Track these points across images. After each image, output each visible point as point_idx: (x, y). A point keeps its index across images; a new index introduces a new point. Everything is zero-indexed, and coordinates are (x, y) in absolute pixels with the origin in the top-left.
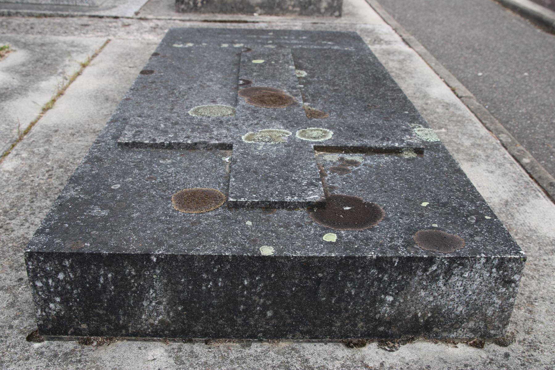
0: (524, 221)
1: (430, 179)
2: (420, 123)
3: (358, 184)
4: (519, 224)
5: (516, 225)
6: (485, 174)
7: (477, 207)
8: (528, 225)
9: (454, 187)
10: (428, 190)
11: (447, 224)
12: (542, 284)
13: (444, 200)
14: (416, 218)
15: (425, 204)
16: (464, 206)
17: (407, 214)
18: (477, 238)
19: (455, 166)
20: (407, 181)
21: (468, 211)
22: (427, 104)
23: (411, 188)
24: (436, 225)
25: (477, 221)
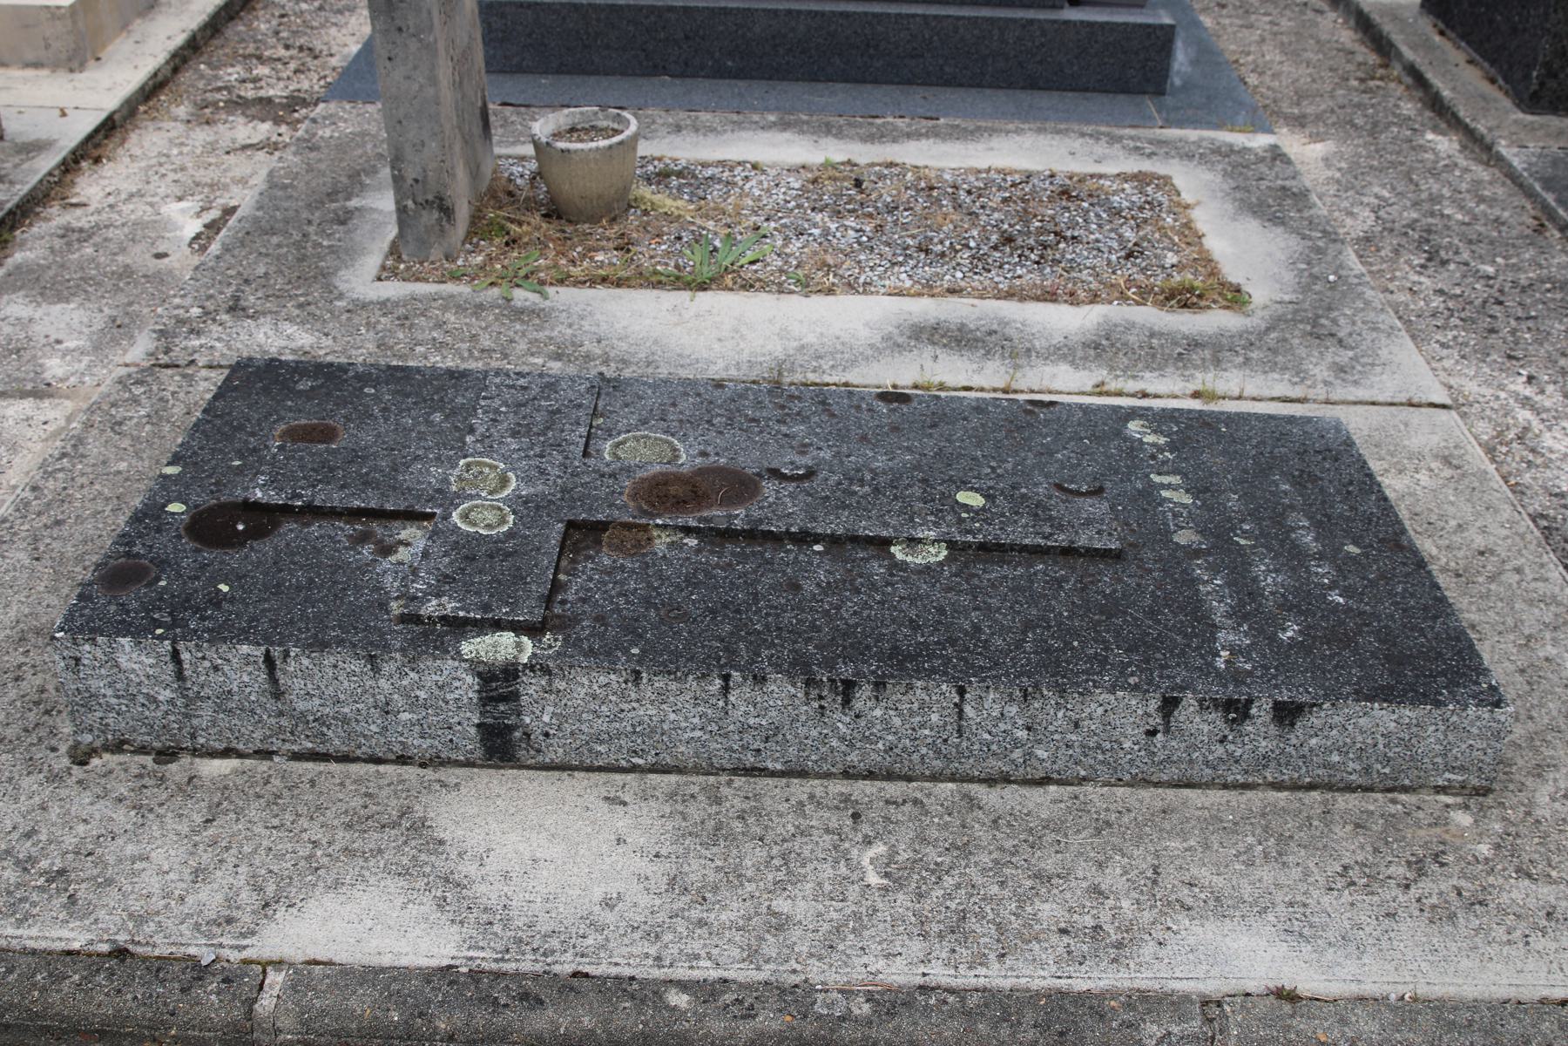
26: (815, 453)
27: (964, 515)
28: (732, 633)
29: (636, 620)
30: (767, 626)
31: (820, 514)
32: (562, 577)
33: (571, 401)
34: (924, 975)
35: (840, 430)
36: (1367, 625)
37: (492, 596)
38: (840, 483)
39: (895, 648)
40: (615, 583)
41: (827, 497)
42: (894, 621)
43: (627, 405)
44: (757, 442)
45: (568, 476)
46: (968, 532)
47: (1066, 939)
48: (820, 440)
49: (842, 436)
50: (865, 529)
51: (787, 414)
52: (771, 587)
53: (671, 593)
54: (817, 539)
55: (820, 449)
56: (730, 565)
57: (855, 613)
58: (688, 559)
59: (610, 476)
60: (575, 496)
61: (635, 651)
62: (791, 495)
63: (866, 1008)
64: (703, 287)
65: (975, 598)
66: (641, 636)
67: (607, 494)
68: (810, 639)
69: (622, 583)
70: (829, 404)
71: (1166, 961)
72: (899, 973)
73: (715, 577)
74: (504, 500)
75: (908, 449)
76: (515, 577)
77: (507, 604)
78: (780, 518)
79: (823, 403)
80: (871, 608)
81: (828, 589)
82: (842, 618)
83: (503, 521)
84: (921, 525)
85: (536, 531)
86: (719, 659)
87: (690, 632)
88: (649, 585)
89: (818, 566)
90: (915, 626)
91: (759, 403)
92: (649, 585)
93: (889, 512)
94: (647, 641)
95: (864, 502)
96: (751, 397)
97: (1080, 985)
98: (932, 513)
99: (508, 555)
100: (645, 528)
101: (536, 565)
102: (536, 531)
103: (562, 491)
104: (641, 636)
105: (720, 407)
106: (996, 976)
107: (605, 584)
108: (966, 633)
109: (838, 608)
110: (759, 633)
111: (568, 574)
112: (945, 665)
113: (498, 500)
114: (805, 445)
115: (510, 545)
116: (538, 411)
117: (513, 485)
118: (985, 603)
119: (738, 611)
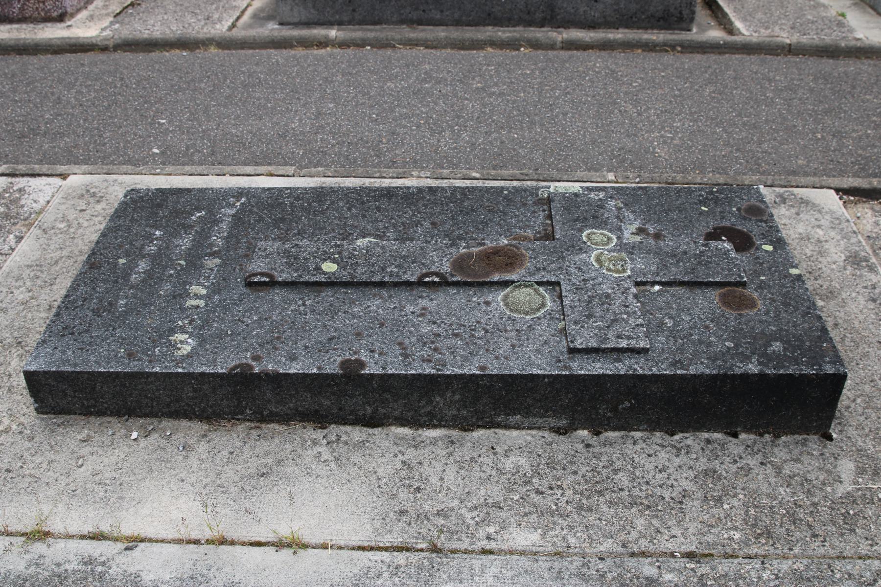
26: (416, 310)
27: (337, 256)
28: (463, 201)
29: (508, 205)
30: (447, 205)
31: (418, 251)
32: (549, 222)
33: (583, 327)
35: (398, 330)
37: (576, 201)
38: (404, 272)
39: (390, 199)
40: (522, 221)
41: (413, 263)
42: (388, 210)
43: (546, 342)
44: (454, 315)
45: (564, 268)
46: (338, 246)
48: (412, 320)
49: (397, 325)
50: (395, 244)
51: (433, 342)
52: (445, 223)
53: (494, 218)
55: (413, 313)
56: (467, 233)
57: (405, 213)
58: (488, 235)
59: (540, 269)
60: (555, 255)
61: (506, 192)
62: (433, 262)
63: (413, 173)
65: (345, 223)
66: (505, 198)
67: (538, 257)
68: (428, 201)
69: (518, 221)
70: (401, 355)
73: (474, 227)
74: (593, 250)
75: (354, 316)
76: (569, 209)
77: (567, 197)
78: (441, 248)
79: (406, 356)
80: (397, 216)
81: (417, 224)
82: (412, 210)
83: (588, 236)
84: (363, 249)
85: (569, 233)
86: (469, 191)
87: (483, 201)
88: (505, 221)
89: (421, 235)
90: (378, 209)
91: (452, 353)
92: (505, 221)
93: (379, 255)
94: (501, 197)
95: (392, 260)
96: (458, 358)
98: (355, 256)
99: (577, 220)
101: (562, 216)
102: (569, 233)
103: (563, 258)
104: (505, 198)
105: (480, 347)
107: (527, 220)
108: (355, 207)
109: (414, 215)
110: (451, 202)
111: (547, 224)
112: (369, 193)
113: (597, 249)
114: (422, 315)
115: (579, 225)
116: (601, 317)
117: (593, 260)
118: (341, 221)
119: (461, 211)
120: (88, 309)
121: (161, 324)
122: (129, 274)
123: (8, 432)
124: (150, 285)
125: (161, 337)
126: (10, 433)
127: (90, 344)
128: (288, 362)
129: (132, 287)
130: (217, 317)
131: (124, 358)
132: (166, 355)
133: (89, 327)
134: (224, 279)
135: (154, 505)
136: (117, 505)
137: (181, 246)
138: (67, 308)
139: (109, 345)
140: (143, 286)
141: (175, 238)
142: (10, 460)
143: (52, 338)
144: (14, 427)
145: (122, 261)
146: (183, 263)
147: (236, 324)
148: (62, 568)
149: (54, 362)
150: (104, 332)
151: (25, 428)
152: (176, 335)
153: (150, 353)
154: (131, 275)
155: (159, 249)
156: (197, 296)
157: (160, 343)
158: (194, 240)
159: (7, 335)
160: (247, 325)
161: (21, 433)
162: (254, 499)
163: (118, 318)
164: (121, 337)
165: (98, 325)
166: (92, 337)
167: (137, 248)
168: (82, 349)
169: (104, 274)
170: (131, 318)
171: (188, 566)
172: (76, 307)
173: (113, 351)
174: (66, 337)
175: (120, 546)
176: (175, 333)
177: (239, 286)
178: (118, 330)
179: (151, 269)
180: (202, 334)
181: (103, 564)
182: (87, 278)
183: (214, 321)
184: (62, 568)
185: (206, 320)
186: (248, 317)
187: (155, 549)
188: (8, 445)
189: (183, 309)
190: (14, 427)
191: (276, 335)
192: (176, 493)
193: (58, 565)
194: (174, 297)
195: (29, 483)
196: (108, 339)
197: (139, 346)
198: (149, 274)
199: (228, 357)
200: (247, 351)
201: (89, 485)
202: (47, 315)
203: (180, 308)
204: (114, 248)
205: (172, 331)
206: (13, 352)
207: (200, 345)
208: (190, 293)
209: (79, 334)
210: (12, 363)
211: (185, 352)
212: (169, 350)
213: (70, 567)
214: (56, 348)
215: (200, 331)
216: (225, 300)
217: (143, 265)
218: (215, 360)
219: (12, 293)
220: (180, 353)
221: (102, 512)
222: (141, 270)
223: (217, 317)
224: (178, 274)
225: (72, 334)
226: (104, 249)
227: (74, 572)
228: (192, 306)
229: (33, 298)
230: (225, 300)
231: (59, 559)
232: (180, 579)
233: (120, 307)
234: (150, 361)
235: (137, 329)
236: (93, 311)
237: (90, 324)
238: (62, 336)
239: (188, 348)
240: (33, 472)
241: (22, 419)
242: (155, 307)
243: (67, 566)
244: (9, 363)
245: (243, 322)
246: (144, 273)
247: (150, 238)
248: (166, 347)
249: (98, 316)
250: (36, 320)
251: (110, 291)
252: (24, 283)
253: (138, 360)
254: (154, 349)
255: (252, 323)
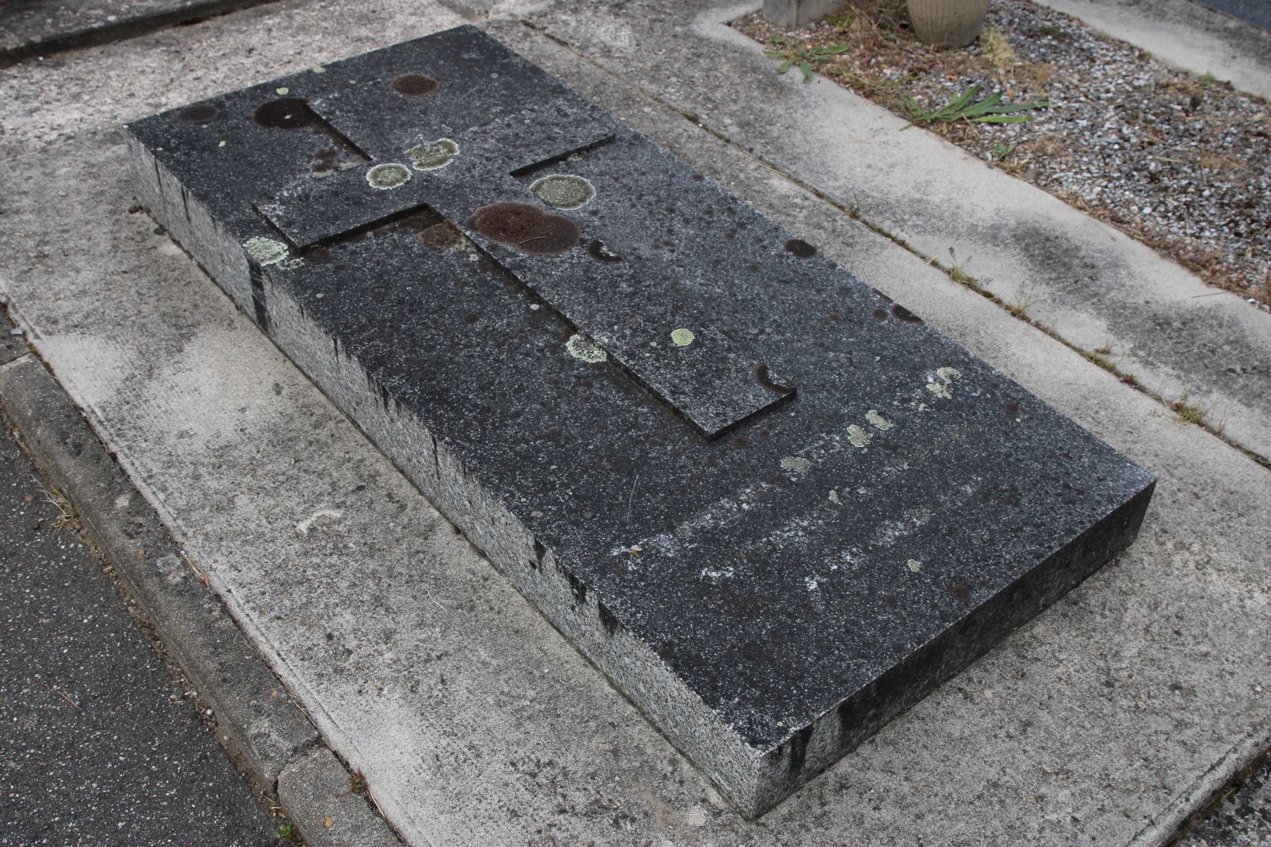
0: (124, 350)
1: (229, 175)
2: (285, 273)
3: (297, 146)
4: (131, 342)
5: (134, 339)
6: (192, 424)
7: (173, 157)
8: (118, 346)
9: (202, 173)
10: (226, 160)
11: (195, 131)
12: (102, 270)
13: (206, 154)
14: (224, 127)
15: (222, 144)
16: (185, 154)
17: (233, 128)
18: (166, 126)
19: (209, 204)
20: (251, 164)
21: (179, 150)
22: (388, 636)
23: (244, 157)
24: (204, 126)
25: (169, 142)
34: (229, 591)
36: (790, 615)
47: (322, 642)
54: (539, 301)
64: (922, 124)
71: (343, 702)
72: (220, 578)
97: (281, 669)
100: (458, 232)
106: (253, 624)
120: (1021, 512)
121: (945, 423)
122: (922, 531)
123: (1181, 543)
124: (910, 489)
125: (959, 407)
126: (1178, 539)
127: (1052, 455)
128: (854, 290)
129: (937, 504)
130: (871, 386)
131: (1023, 410)
132: (972, 381)
133: (1038, 482)
134: (809, 428)
135: (1055, 373)
136: (1092, 395)
137: (804, 529)
138: (1050, 535)
139: (1029, 439)
140: (921, 496)
141: (798, 552)
142: (1190, 507)
143: (1098, 498)
144: (1170, 545)
145: (914, 566)
146: (833, 496)
147: (859, 363)
148: (1176, 373)
149: (1112, 462)
150: (1024, 459)
151: (1156, 534)
152: (940, 396)
153: (988, 396)
154: (922, 529)
155: (840, 549)
156: (867, 426)
157: (967, 399)
158: (776, 526)
159: (1122, 715)
160: (850, 353)
161: (1165, 532)
162: (959, 323)
163: (991, 469)
164: (1008, 439)
165: (1025, 476)
166: (1044, 464)
167: (872, 576)
168: (1067, 456)
169: (958, 560)
170: (976, 455)
171: (1061, 313)
172: (1037, 526)
173: (1029, 427)
174: (1079, 487)
175: (1111, 360)
176: (939, 399)
177: (804, 406)
178: (1004, 450)
179: (884, 517)
180: (909, 377)
181: (1135, 355)
182: (989, 572)
183: (880, 383)
184: (1176, 373)
185: (888, 390)
186: (838, 361)
187: (1081, 340)
188: (1186, 527)
189: (901, 424)
190: (1170, 545)
191: (833, 322)
192: (1028, 369)
193: (1178, 377)
194: (895, 448)
195: (1176, 468)
196: (1025, 447)
197: (994, 413)
198: (895, 513)
199: (908, 335)
200: (881, 327)
201: (1112, 428)
202: (1040, 713)
203: (903, 427)
204: (904, 607)
205: (941, 404)
206: (1126, 674)
207: (924, 367)
208: (872, 439)
209: (1057, 480)
210: (1135, 651)
211: (949, 370)
212: (964, 385)
213: (1168, 369)
214: (1100, 480)
215: (908, 383)
216: (839, 400)
217: (891, 534)
218: (925, 341)
219: (1075, 820)
220: (955, 372)
221: (1112, 398)
222: (900, 525)
223: (871, 386)
224: (856, 481)
225: (1066, 486)
226: (922, 616)
227: (1166, 364)
228: (886, 419)
229: (1045, 773)
230: (839, 400)
231: (1175, 382)
232: (1074, 308)
233: (977, 483)
234: (996, 386)
235: (980, 435)
236: (1017, 504)
237: (1036, 485)
238: (1080, 492)
239: (941, 372)
240: (1168, 477)
241: (1156, 548)
242: (932, 451)
243: (1171, 372)
244: (1139, 653)
245: (850, 360)
246: (900, 518)
247: (833, 588)
248: (963, 389)
249: (1015, 489)
250: (1063, 714)
251: (969, 521)
252: (1041, 830)
253: (1008, 396)
254: (980, 397)
255: (842, 352)
